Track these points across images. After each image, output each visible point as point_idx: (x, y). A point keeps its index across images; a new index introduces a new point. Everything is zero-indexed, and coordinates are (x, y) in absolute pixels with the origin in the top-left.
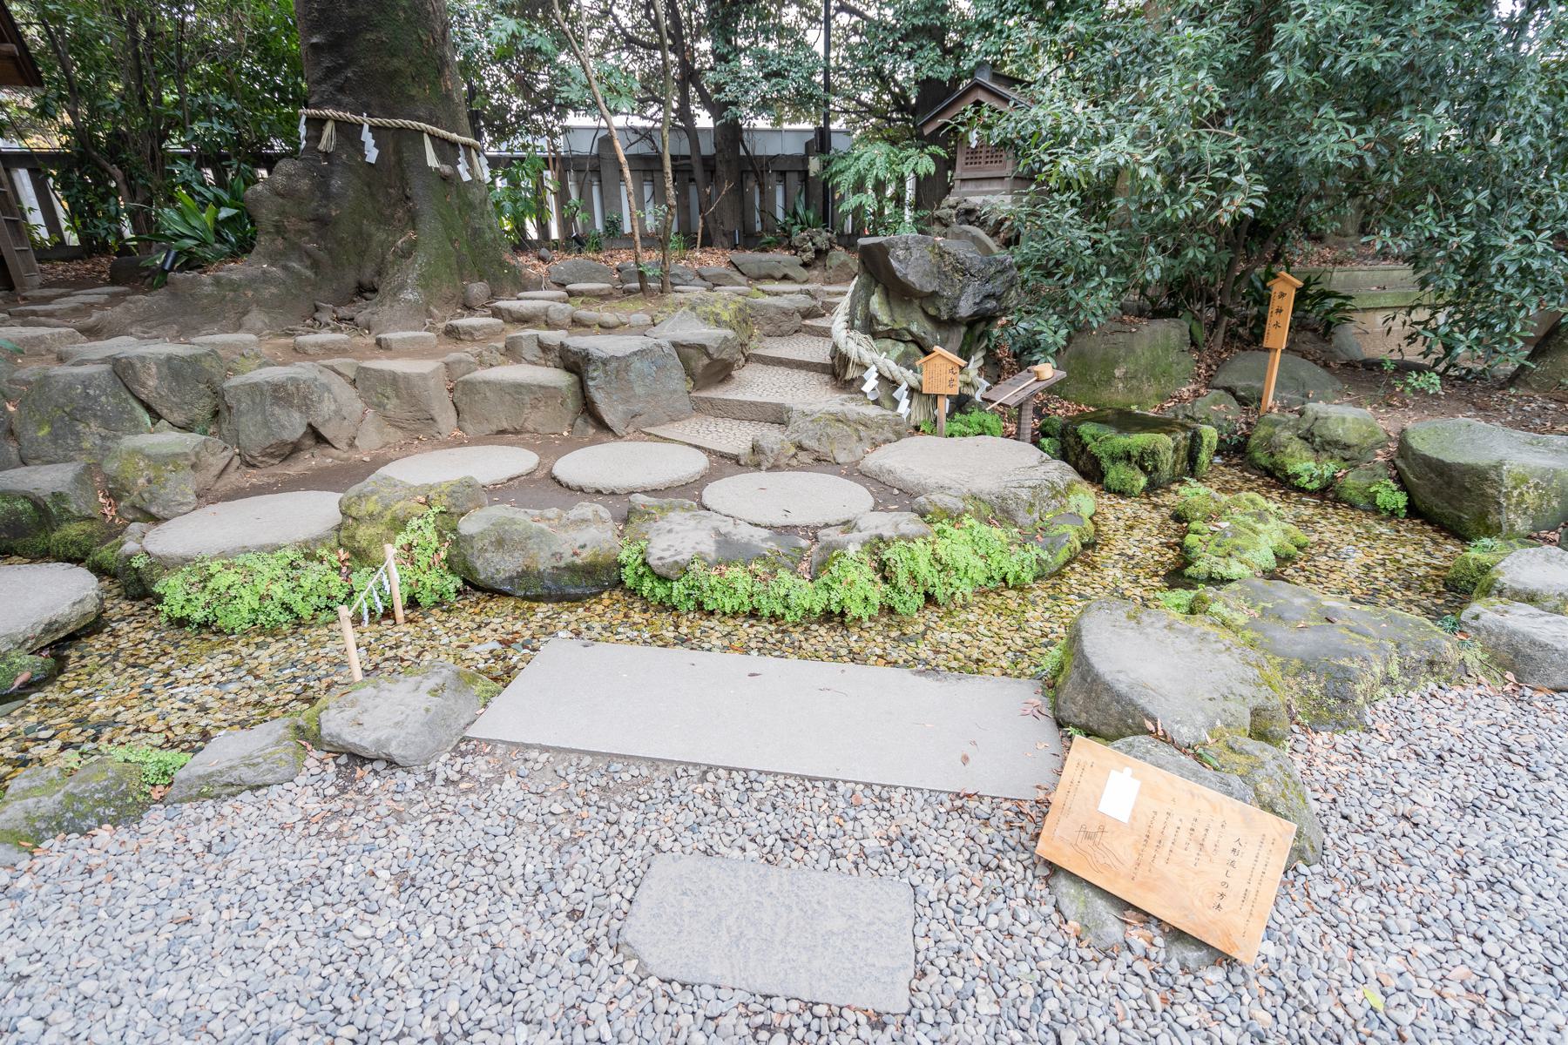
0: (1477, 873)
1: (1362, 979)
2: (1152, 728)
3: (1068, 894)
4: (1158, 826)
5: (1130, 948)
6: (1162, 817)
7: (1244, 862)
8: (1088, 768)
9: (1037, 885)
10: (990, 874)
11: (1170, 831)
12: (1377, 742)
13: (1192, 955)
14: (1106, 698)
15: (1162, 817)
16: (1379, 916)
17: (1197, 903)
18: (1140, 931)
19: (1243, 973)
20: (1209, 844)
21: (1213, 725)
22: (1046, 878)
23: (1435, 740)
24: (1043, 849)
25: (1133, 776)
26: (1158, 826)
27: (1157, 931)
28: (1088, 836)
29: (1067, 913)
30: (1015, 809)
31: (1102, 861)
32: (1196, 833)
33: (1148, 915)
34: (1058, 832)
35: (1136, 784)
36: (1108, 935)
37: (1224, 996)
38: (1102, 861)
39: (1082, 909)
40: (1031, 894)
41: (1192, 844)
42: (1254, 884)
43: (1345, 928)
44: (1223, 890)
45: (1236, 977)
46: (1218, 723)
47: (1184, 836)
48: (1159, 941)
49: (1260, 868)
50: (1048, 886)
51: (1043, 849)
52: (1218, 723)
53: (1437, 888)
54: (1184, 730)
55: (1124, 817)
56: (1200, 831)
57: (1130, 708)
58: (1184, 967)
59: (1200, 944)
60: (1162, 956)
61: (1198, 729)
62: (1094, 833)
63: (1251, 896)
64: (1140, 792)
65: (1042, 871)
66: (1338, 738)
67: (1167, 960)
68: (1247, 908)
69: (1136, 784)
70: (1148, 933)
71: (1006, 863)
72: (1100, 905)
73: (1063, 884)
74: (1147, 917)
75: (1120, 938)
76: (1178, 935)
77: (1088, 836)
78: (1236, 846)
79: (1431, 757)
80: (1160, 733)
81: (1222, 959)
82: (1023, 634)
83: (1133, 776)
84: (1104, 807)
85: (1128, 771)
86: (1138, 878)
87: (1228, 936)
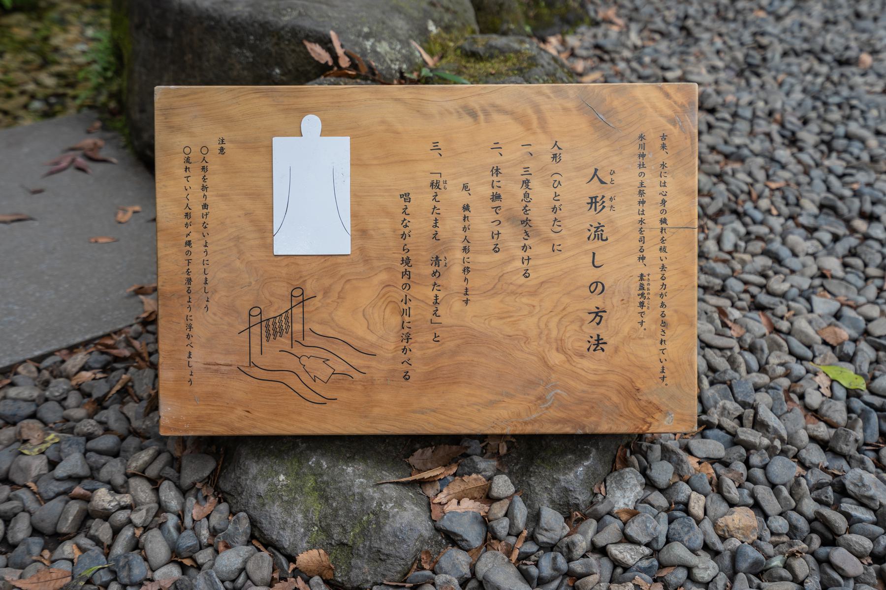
0: (809, 137)
1: (809, 354)
2: (324, 57)
3: (274, 491)
4: (420, 225)
5: (452, 539)
6: (423, 200)
7: (622, 215)
8: (214, 163)
9: (195, 510)
10: (68, 549)
11: (451, 225)
12: (614, 30)
13: (575, 476)
14: (216, 49)
15: (423, 200)
16: (758, 246)
17: (556, 358)
18: (457, 486)
19: (667, 454)
20: (539, 215)
21: (425, 31)
22: (212, 481)
23: (667, 13)
24: (175, 416)
25: (328, 130)
26: (420, 225)
27: (486, 465)
28: (273, 329)
29: (286, 539)
30: (98, 359)
31: (324, 372)
32: (506, 203)
33: (456, 439)
34: (199, 356)
35: (342, 144)
36: (398, 538)
37: (662, 528)
38: (324, 372)
39: (317, 508)
40: (187, 541)
41: (506, 231)
42: (652, 254)
43: (735, 285)
44: (596, 302)
45: (663, 472)
46: (432, 28)
47: (482, 221)
48: (503, 485)
49: (652, 215)
50: (222, 497)
51: (175, 416)
52: (432, 28)
53: (786, 175)
54: (383, 47)
55: (341, 243)
56: (513, 190)
57: (268, 44)
58: (572, 514)
59: (575, 444)
60: (521, 512)
61: (405, 43)
62: (289, 304)
63: (654, 287)
64: (357, 163)
65: (195, 471)
66: (573, 41)
67: (535, 518)
68: (652, 315)
69: (342, 144)
70: (474, 481)
71: (103, 498)
72: (354, 476)
73: (263, 479)
74: (456, 449)
75: (424, 528)
76: (528, 452)
77: (273, 329)
78: (595, 189)
79: (675, 31)
80: (344, 62)
81: (626, 450)
82: (56, 69)
83: (328, 130)
84: (285, 244)
85: (311, 123)
86: (418, 369)
87: (632, 392)
